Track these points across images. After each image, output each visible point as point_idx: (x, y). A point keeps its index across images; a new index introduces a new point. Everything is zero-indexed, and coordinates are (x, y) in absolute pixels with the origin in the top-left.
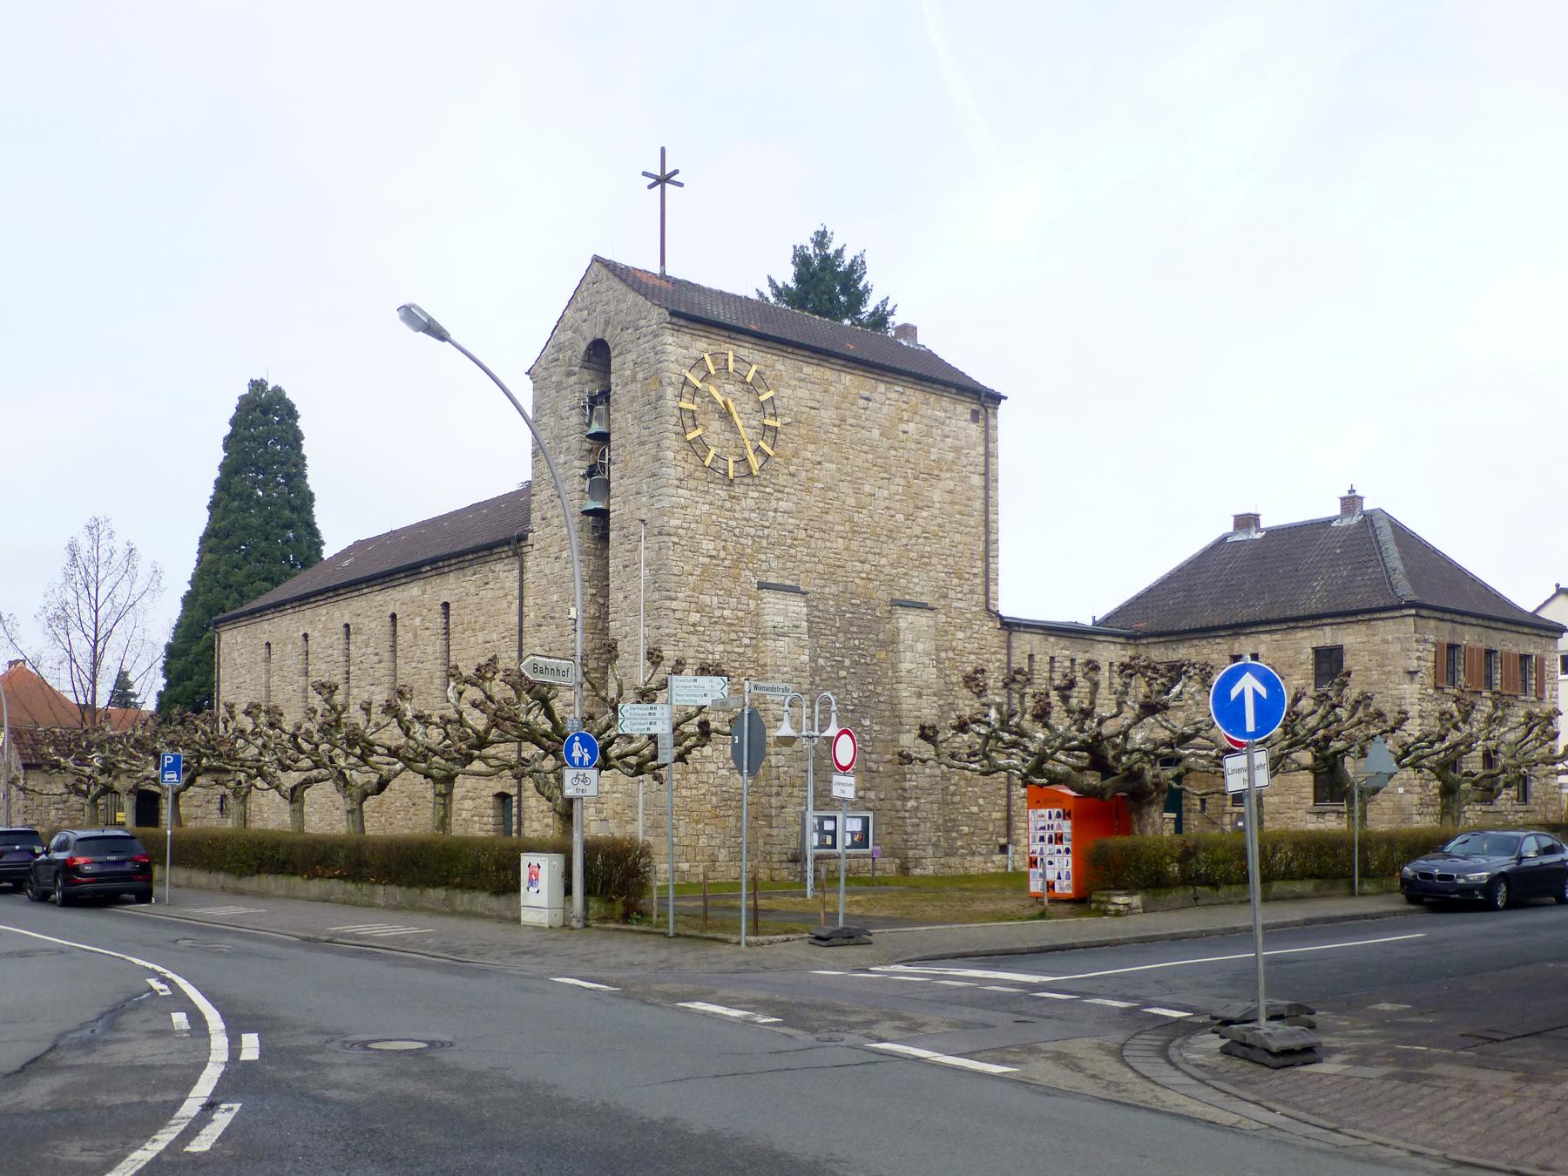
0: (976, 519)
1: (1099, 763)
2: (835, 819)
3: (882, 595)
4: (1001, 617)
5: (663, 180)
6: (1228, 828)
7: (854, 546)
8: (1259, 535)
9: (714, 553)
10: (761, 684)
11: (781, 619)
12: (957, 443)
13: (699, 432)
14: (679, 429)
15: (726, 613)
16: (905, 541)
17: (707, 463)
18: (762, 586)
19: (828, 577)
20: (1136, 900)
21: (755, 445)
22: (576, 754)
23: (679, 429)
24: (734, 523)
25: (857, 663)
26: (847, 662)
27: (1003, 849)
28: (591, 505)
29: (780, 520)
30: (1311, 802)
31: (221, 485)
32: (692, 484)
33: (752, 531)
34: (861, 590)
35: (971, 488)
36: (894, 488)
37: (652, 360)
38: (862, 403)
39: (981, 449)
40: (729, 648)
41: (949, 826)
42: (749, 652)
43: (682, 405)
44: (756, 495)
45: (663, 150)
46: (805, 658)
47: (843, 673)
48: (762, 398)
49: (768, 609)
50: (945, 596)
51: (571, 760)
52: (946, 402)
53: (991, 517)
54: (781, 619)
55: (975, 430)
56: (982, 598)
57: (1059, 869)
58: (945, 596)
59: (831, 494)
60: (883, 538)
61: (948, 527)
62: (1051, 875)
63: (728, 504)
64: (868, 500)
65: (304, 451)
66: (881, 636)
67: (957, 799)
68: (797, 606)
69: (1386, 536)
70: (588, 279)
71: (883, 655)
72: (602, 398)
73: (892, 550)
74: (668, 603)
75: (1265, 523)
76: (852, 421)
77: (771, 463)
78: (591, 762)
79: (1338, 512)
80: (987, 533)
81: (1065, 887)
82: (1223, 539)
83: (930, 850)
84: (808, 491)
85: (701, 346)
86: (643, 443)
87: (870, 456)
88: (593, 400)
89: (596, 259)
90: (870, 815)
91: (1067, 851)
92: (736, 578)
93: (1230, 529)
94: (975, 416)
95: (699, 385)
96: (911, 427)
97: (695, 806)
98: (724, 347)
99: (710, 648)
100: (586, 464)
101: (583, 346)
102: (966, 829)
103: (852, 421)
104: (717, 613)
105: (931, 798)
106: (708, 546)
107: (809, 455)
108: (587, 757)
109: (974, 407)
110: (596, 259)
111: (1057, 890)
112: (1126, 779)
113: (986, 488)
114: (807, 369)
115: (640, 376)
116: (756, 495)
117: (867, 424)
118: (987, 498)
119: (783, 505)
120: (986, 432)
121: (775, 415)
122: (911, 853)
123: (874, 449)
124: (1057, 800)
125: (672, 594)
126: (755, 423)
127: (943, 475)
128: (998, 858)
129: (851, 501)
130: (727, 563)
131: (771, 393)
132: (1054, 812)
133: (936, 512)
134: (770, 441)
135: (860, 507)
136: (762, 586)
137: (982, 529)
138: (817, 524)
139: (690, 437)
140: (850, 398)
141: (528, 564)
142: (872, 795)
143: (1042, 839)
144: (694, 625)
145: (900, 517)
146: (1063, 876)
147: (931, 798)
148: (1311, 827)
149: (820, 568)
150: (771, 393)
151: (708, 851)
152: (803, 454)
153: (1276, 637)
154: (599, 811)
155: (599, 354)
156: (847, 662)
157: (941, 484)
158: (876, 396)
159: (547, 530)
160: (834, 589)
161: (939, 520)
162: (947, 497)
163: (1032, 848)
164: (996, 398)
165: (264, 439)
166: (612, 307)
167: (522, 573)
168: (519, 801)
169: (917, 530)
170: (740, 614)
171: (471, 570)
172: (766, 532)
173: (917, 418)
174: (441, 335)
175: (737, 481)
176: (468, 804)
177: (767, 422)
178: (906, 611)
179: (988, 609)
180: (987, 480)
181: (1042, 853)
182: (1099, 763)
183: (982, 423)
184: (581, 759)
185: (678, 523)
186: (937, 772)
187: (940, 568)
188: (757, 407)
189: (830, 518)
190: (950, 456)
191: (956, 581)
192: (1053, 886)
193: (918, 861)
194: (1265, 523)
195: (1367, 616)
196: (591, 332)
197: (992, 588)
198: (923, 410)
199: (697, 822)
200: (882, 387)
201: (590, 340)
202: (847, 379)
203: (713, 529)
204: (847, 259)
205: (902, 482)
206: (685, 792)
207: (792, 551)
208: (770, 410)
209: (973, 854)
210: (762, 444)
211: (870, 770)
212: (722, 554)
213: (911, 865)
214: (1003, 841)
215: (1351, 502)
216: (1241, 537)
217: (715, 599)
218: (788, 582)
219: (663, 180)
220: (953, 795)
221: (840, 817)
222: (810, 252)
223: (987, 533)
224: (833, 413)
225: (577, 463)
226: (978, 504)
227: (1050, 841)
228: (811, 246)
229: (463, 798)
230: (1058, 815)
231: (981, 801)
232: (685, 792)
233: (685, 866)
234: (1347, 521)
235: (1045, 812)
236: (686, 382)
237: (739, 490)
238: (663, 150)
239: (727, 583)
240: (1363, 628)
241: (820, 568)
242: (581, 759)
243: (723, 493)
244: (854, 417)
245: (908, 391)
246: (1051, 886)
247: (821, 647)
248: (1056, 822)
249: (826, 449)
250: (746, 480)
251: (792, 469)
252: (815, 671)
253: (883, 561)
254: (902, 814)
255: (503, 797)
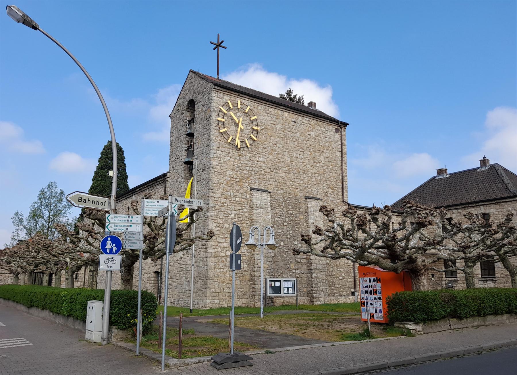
0: (338, 168)
1: (393, 256)
2: (280, 281)
3: (302, 194)
4: (349, 204)
5: (218, 46)
6: (445, 286)
7: (290, 175)
8: (447, 176)
9: (232, 176)
10: (180, 199)
11: (259, 202)
12: (330, 140)
13: (225, 129)
14: (218, 128)
15: (237, 199)
16: (310, 175)
17: (229, 141)
18: (252, 189)
19: (280, 187)
20: (419, 328)
21: (249, 136)
22: (108, 246)
23: (218, 128)
24: (240, 165)
25: (292, 220)
26: (287, 219)
27: (353, 294)
28: (187, 160)
29: (260, 164)
30: (480, 276)
31: (96, 173)
32: (223, 149)
33: (248, 168)
34: (292, 192)
35: (336, 156)
36: (305, 155)
37: (208, 103)
38: (293, 123)
39: (340, 143)
40: (238, 213)
41: (331, 284)
42: (247, 214)
43: (218, 119)
44: (250, 155)
45: (218, 35)
46: (269, 217)
47: (285, 224)
48: (252, 119)
49: (254, 197)
50: (327, 196)
51: (105, 250)
52: (325, 125)
53: (344, 167)
54: (259, 202)
55: (337, 136)
56: (341, 197)
57: (376, 308)
58: (327, 196)
59: (280, 156)
60: (301, 173)
61: (327, 170)
62: (372, 310)
63: (238, 158)
64: (295, 159)
65: (125, 162)
66: (301, 210)
67: (333, 273)
68: (266, 197)
69: (501, 172)
70: (189, 79)
71: (302, 217)
72: (192, 121)
73: (305, 178)
74: (212, 194)
75: (449, 172)
76: (289, 130)
77: (256, 143)
78: (117, 251)
79: (479, 166)
80: (342, 173)
81: (379, 317)
82: (433, 178)
83: (323, 294)
84: (271, 154)
85: (228, 98)
86: (204, 134)
87: (296, 143)
88: (190, 122)
89: (191, 71)
90: (295, 280)
91: (380, 298)
92: (241, 186)
93: (436, 175)
94: (337, 130)
95: (226, 112)
96: (312, 133)
97: (223, 276)
98: (237, 99)
99: (230, 212)
100: (187, 146)
101: (187, 103)
102: (337, 286)
103: (289, 130)
104: (233, 199)
105: (322, 273)
106: (229, 173)
107: (271, 141)
108: (115, 249)
109: (336, 127)
110: (191, 71)
111: (375, 318)
112: (408, 263)
113: (342, 156)
114: (271, 110)
115: (204, 110)
116: (250, 155)
117: (294, 131)
118: (342, 160)
119: (260, 159)
120: (341, 137)
121: (257, 126)
122: (314, 295)
123: (297, 140)
124: (371, 273)
125: (214, 191)
126: (249, 128)
127: (325, 151)
128: (351, 297)
129: (289, 159)
130: (237, 180)
131: (256, 117)
132: (372, 279)
133: (322, 164)
134: (255, 135)
135: (292, 162)
136: (252, 189)
137: (340, 172)
138: (274, 167)
139: (221, 131)
140: (288, 121)
141: (168, 185)
142: (298, 271)
143: (366, 292)
144: (223, 203)
145: (308, 166)
146: (378, 311)
147: (322, 273)
148: (481, 286)
149: (276, 183)
150: (256, 117)
151: (228, 295)
152: (269, 140)
153: (460, 211)
154: (187, 278)
155: (192, 104)
156: (287, 219)
157: (324, 155)
158: (298, 121)
159: (174, 171)
160: (282, 192)
161: (324, 168)
162: (327, 160)
163: (362, 296)
164: (345, 125)
165: (111, 158)
166: (196, 86)
167: (165, 188)
168: (161, 275)
169: (315, 171)
170: (243, 200)
171: (151, 189)
172: (254, 169)
173: (314, 130)
174: (35, 28)
175: (242, 149)
176: (146, 276)
177: (254, 127)
178: (311, 200)
179: (343, 201)
180: (342, 154)
181: (367, 299)
182: (393, 256)
183: (340, 133)
184: (111, 250)
185: (217, 163)
186: (325, 263)
187: (324, 185)
188: (250, 122)
189: (280, 165)
190: (328, 145)
191: (330, 190)
192: (373, 316)
193: (317, 298)
194: (449, 172)
195: (500, 201)
196: (189, 97)
197: (345, 193)
198: (317, 127)
199: (223, 283)
200: (300, 118)
201: (188, 100)
202: (286, 114)
203: (232, 167)
204: (297, 98)
205: (309, 153)
206: (218, 270)
207: (264, 176)
208: (255, 123)
209: (341, 295)
210: (252, 135)
211: (297, 262)
212: (235, 176)
213: (315, 300)
214: (353, 290)
215: (484, 162)
216: (440, 177)
217: (232, 194)
218: (263, 188)
219: (218, 46)
220: (332, 272)
221: (282, 280)
222: (286, 96)
223: (342, 173)
224: (281, 126)
225: (184, 146)
226: (339, 163)
227: (371, 293)
228: (286, 95)
229: (145, 274)
230: (374, 281)
231: (343, 275)
232: (218, 270)
233: (217, 301)
234: (483, 169)
235: (368, 279)
236: (220, 111)
237: (242, 153)
238: (218, 35)
239: (238, 188)
240: (498, 206)
241: (276, 183)
242: (111, 250)
243: (236, 154)
244: (289, 128)
245: (311, 120)
246: (372, 316)
247: (277, 213)
248: (373, 284)
249: (278, 139)
250: (246, 149)
251: (265, 146)
252: (274, 223)
253: (302, 182)
254: (311, 279)
255: (157, 272)
